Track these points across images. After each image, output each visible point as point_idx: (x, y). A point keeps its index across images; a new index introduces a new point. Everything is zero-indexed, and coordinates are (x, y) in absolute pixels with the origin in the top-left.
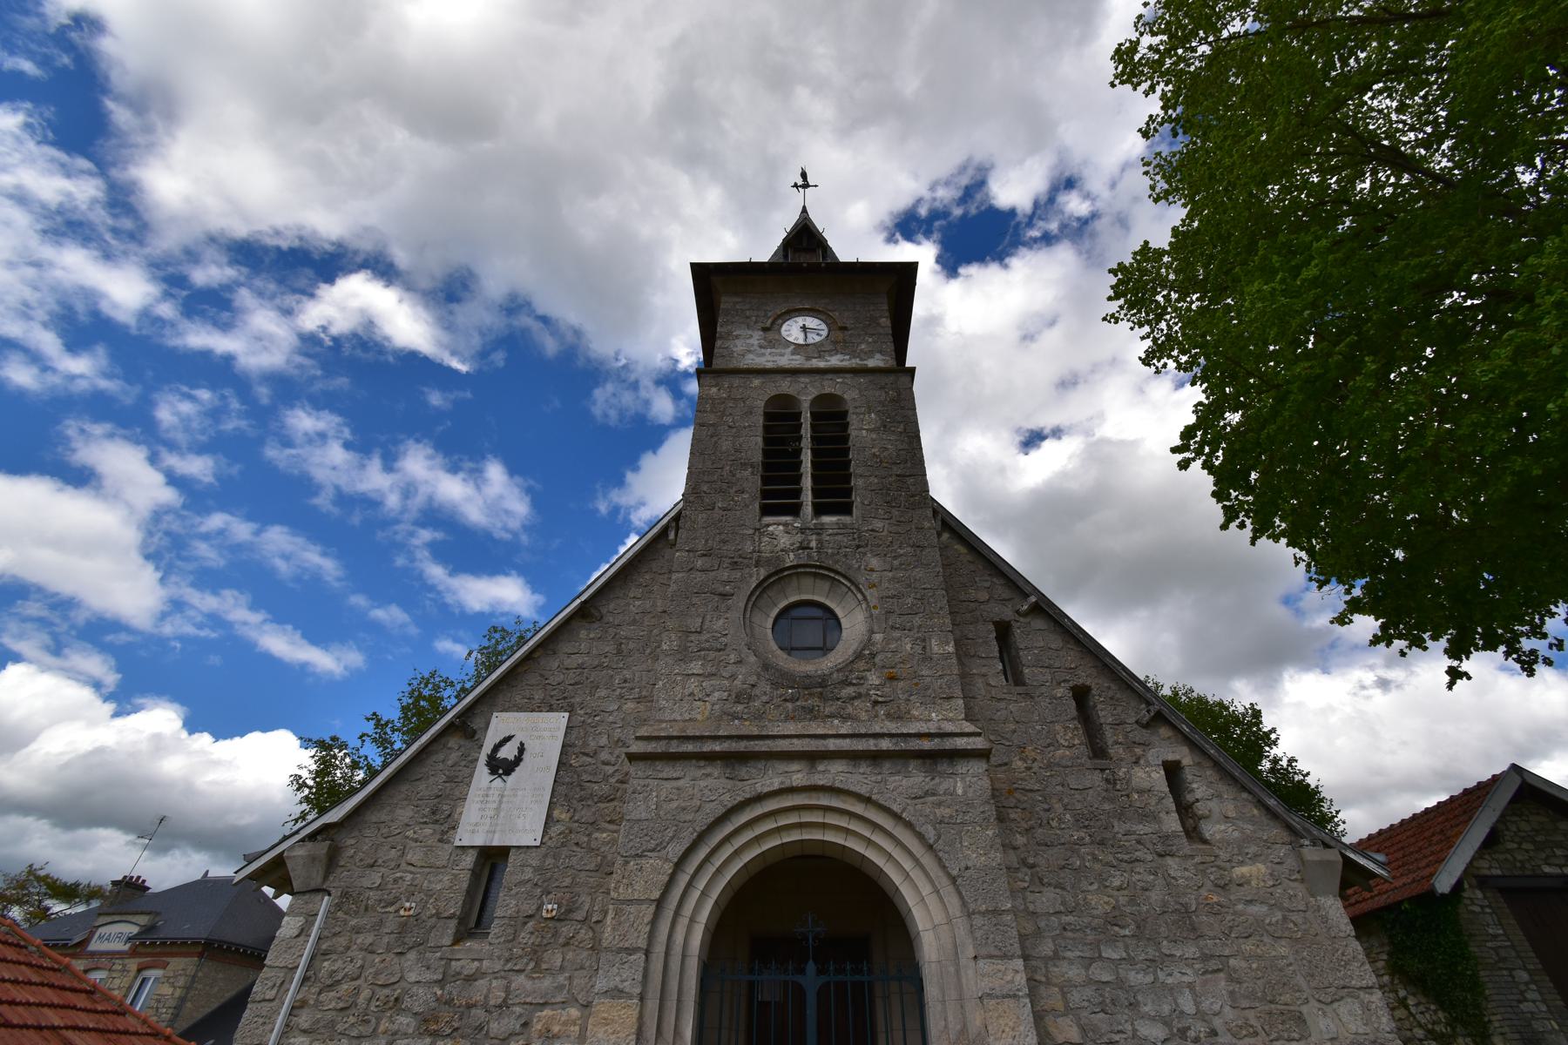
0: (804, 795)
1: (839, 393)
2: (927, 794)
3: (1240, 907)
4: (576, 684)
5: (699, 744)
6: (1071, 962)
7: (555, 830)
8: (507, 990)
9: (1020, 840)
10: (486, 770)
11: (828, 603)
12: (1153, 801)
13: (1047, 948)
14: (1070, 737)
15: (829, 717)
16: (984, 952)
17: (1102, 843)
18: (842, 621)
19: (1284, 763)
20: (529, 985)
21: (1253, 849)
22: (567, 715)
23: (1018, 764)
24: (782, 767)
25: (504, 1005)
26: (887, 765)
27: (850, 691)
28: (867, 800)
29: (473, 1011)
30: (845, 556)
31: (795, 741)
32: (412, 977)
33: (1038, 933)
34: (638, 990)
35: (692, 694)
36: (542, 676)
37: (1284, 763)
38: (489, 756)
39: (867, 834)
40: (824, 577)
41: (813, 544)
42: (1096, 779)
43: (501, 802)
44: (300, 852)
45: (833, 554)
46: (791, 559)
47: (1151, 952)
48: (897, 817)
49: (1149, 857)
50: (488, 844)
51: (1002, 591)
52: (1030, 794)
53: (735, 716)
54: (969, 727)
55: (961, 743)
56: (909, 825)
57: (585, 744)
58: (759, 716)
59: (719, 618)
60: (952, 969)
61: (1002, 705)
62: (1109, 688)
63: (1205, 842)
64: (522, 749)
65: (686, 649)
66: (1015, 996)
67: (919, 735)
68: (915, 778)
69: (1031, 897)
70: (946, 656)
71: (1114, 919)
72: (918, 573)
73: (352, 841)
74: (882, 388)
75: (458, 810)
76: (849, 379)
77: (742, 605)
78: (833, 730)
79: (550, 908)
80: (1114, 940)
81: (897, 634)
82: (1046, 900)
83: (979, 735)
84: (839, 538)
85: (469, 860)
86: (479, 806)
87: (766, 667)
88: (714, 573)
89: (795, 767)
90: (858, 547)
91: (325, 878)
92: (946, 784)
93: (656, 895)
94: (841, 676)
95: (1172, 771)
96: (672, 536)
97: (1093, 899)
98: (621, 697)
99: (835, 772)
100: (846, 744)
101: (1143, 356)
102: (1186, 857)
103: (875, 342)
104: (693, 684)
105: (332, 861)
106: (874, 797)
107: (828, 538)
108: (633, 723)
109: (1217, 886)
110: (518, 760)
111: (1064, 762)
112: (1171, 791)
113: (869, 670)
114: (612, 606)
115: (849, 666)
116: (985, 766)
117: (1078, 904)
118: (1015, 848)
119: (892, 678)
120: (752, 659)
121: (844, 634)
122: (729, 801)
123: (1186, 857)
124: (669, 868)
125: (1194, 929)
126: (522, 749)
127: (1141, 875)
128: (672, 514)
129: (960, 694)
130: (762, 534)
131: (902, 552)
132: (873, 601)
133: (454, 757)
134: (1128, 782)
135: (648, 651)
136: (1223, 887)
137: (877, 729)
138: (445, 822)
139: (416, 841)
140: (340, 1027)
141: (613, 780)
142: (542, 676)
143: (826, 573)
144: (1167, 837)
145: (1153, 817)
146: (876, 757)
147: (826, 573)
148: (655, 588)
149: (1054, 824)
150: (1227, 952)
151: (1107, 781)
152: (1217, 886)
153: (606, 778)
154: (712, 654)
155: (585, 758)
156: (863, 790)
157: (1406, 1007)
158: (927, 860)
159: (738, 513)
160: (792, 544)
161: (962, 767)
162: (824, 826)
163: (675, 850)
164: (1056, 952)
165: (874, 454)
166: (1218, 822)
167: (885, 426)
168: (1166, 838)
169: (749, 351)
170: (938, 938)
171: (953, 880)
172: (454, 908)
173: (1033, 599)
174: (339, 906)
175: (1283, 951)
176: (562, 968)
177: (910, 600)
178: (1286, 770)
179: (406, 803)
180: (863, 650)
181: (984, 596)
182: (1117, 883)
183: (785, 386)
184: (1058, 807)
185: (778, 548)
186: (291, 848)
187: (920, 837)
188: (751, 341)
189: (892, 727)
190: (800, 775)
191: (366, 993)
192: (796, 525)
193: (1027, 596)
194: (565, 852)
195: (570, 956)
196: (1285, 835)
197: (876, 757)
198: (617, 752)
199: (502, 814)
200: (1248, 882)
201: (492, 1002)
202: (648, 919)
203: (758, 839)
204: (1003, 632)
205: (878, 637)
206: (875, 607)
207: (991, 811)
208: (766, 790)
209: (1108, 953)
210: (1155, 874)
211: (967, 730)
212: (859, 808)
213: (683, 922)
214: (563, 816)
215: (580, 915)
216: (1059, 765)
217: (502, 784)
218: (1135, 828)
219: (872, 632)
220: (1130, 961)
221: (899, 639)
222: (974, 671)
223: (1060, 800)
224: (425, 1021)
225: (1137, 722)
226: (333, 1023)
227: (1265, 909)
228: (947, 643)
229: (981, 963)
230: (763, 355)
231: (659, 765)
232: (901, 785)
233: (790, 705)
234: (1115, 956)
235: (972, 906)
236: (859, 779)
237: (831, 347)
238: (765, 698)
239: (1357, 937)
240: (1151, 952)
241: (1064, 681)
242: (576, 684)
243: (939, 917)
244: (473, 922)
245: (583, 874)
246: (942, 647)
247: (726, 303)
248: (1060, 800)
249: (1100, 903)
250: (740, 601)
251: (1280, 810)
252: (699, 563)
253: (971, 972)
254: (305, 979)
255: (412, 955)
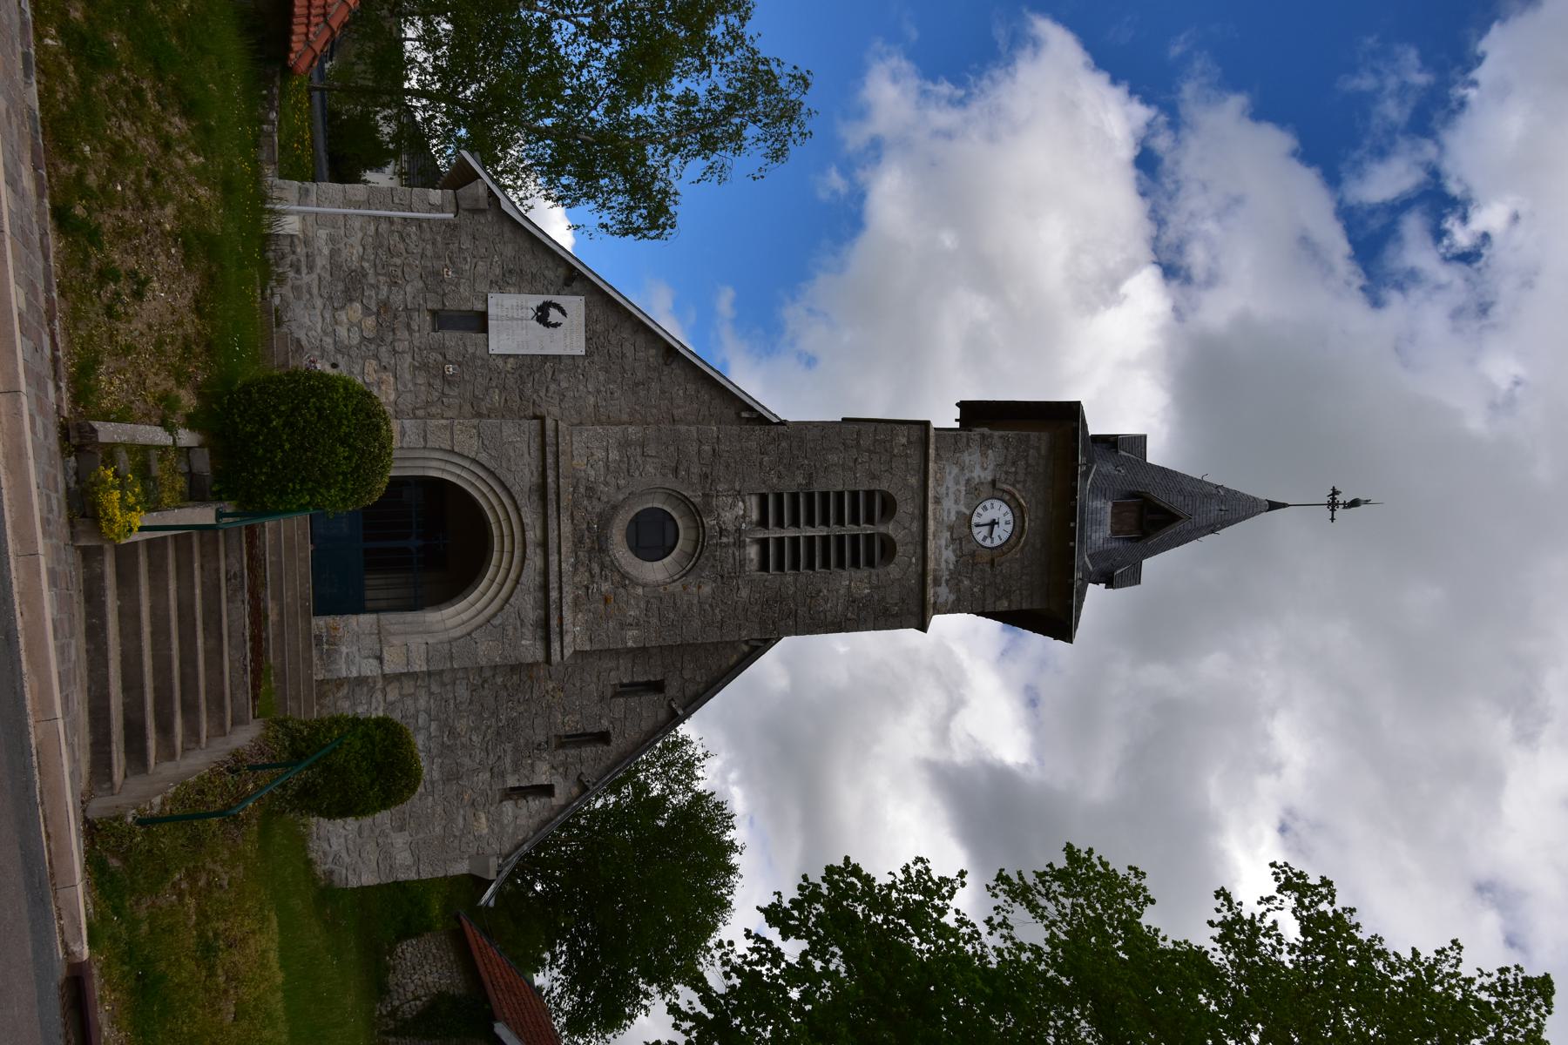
0: (521, 538)
1: (897, 559)
2: (522, 621)
3: (462, 812)
4: (609, 355)
5: (553, 466)
6: (428, 702)
7: (500, 363)
8: (403, 352)
9: (499, 680)
10: (540, 303)
11: (676, 551)
12: (526, 772)
13: (435, 688)
14: (570, 723)
15: (576, 554)
16: (430, 648)
17: (498, 734)
18: (660, 563)
19: (645, 1002)
20: (406, 365)
21: (497, 829)
22: (583, 353)
23: (550, 686)
24: (538, 524)
25: (395, 352)
26: (540, 595)
27: (596, 569)
28: (517, 581)
29: (391, 334)
30: (713, 566)
31: (556, 533)
32: (408, 289)
33: (443, 685)
34: (405, 445)
35: (592, 455)
36: (616, 327)
37: (645, 1002)
38: (550, 302)
39: (497, 580)
40: (696, 548)
41: (724, 540)
42: (541, 738)
43: (517, 319)
44: (481, 191)
45: (714, 557)
46: (710, 522)
47: (435, 751)
48: (507, 600)
49: (490, 763)
50: (490, 317)
51: (691, 689)
52: (529, 690)
53: (575, 488)
54: (568, 652)
55: (556, 646)
56: (502, 608)
57: (561, 371)
58: (575, 505)
59: (656, 468)
60: (421, 629)
61: (595, 679)
62: (609, 759)
63: (501, 801)
64: (556, 325)
65: (629, 446)
66: (408, 664)
67: (561, 618)
68: (532, 614)
69: (465, 682)
70: (624, 641)
71: (452, 733)
72: (696, 624)
73: (490, 218)
74: (903, 601)
75: (512, 289)
76: (914, 569)
77: (667, 485)
78: (565, 559)
79: (450, 369)
80: (440, 729)
81: (642, 605)
82: (463, 692)
83: (562, 658)
84: (731, 560)
85: (479, 307)
86: (515, 304)
87: (615, 508)
88: (696, 460)
89: (539, 532)
90: (722, 577)
91: (468, 210)
92: (528, 634)
93: (456, 449)
94: (607, 563)
95: (547, 790)
96: (745, 415)
97: (464, 721)
98: (599, 392)
99: (535, 560)
100: (554, 567)
101: (1004, 874)
102: (491, 786)
103: (973, 594)
104: (600, 454)
105: (475, 211)
106: (519, 586)
107: (730, 551)
108: (578, 405)
109: (474, 800)
110: (548, 325)
111: (552, 717)
112: (533, 787)
113: (612, 584)
114: (678, 371)
115: (615, 568)
116: (540, 660)
117: (461, 711)
118: (494, 676)
119: (606, 600)
120: (621, 497)
121: (648, 564)
122: (515, 490)
123: (491, 786)
124: (472, 455)
125: (448, 780)
126: (556, 325)
127: (479, 755)
128: (765, 414)
129: (594, 648)
130: (735, 497)
131: (717, 611)
132: (670, 588)
133: (550, 274)
134: (539, 759)
135: (637, 408)
136: (473, 804)
137: (566, 589)
138: (501, 285)
139: (491, 264)
140: (380, 252)
141: (535, 396)
142: (616, 327)
143: (698, 551)
144: (503, 777)
145: (515, 771)
146: (545, 587)
147: (698, 551)
148: (695, 406)
149: (510, 704)
150: (436, 797)
151: (540, 745)
152: (474, 800)
153: (537, 391)
154: (624, 466)
155: (551, 373)
156: (523, 579)
157: (414, 999)
158: (481, 618)
159: (757, 475)
160: (724, 522)
161: (539, 645)
162: (502, 551)
163: (483, 457)
164: (432, 694)
165: (820, 591)
166: (513, 811)
167: (854, 602)
168: (502, 775)
169: (962, 469)
170: (438, 622)
171: (469, 634)
172: (450, 305)
173: (680, 712)
174: (448, 225)
175: (437, 829)
176: (415, 384)
177: (672, 616)
178: (638, 1003)
179: (517, 248)
180: (629, 579)
181: (687, 674)
182: (474, 738)
183: (906, 509)
184: (521, 709)
185: (721, 511)
186: (484, 182)
187: (494, 615)
188: (978, 468)
189: (568, 599)
190: (533, 536)
191: (398, 261)
192: (744, 525)
193: (684, 709)
194: (485, 372)
195: (423, 388)
196: (505, 851)
197: (545, 587)
198: (555, 396)
199: (509, 323)
200: (476, 820)
201: (396, 344)
202: (442, 445)
203: (492, 507)
204: (657, 687)
205: (640, 591)
206: (665, 589)
207: (512, 661)
208: (523, 515)
209: (434, 726)
210: (480, 764)
211: (565, 651)
212: (512, 575)
213: (442, 465)
214: (509, 366)
215: (447, 390)
216: (550, 713)
217: (530, 317)
218: (508, 757)
219: (644, 586)
220: (429, 738)
221: (638, 607)
222: (621, 661)
223: (526, 711)
224: (385, 305)
225: (582, 773)
226: (381, 246)
227: (461, 826)
228: (634, 642)
229: (424, 646)
230: (957, 483)
231: (538, 439)
232: (527, 604)
233: (585, 526)
234: (432, 730)
235: (454, 644)
236: (531, 577)
237: (966, 550)
238: (590, 508)
239: (445, 877)
240: (435, 751)
241: (614, 728)
242: (609, 355)
243: (450, 623)
244: (442, 320)
245: (471, 387)
246: (631, 638)
247: (1039, 440)
248: (526, 711)
249: (462, 725)
250: (671, 483)
251: (520, 851)
252: (706, 448)
253: (419, 640)
254: (405, 219)
255: (421, 284)
